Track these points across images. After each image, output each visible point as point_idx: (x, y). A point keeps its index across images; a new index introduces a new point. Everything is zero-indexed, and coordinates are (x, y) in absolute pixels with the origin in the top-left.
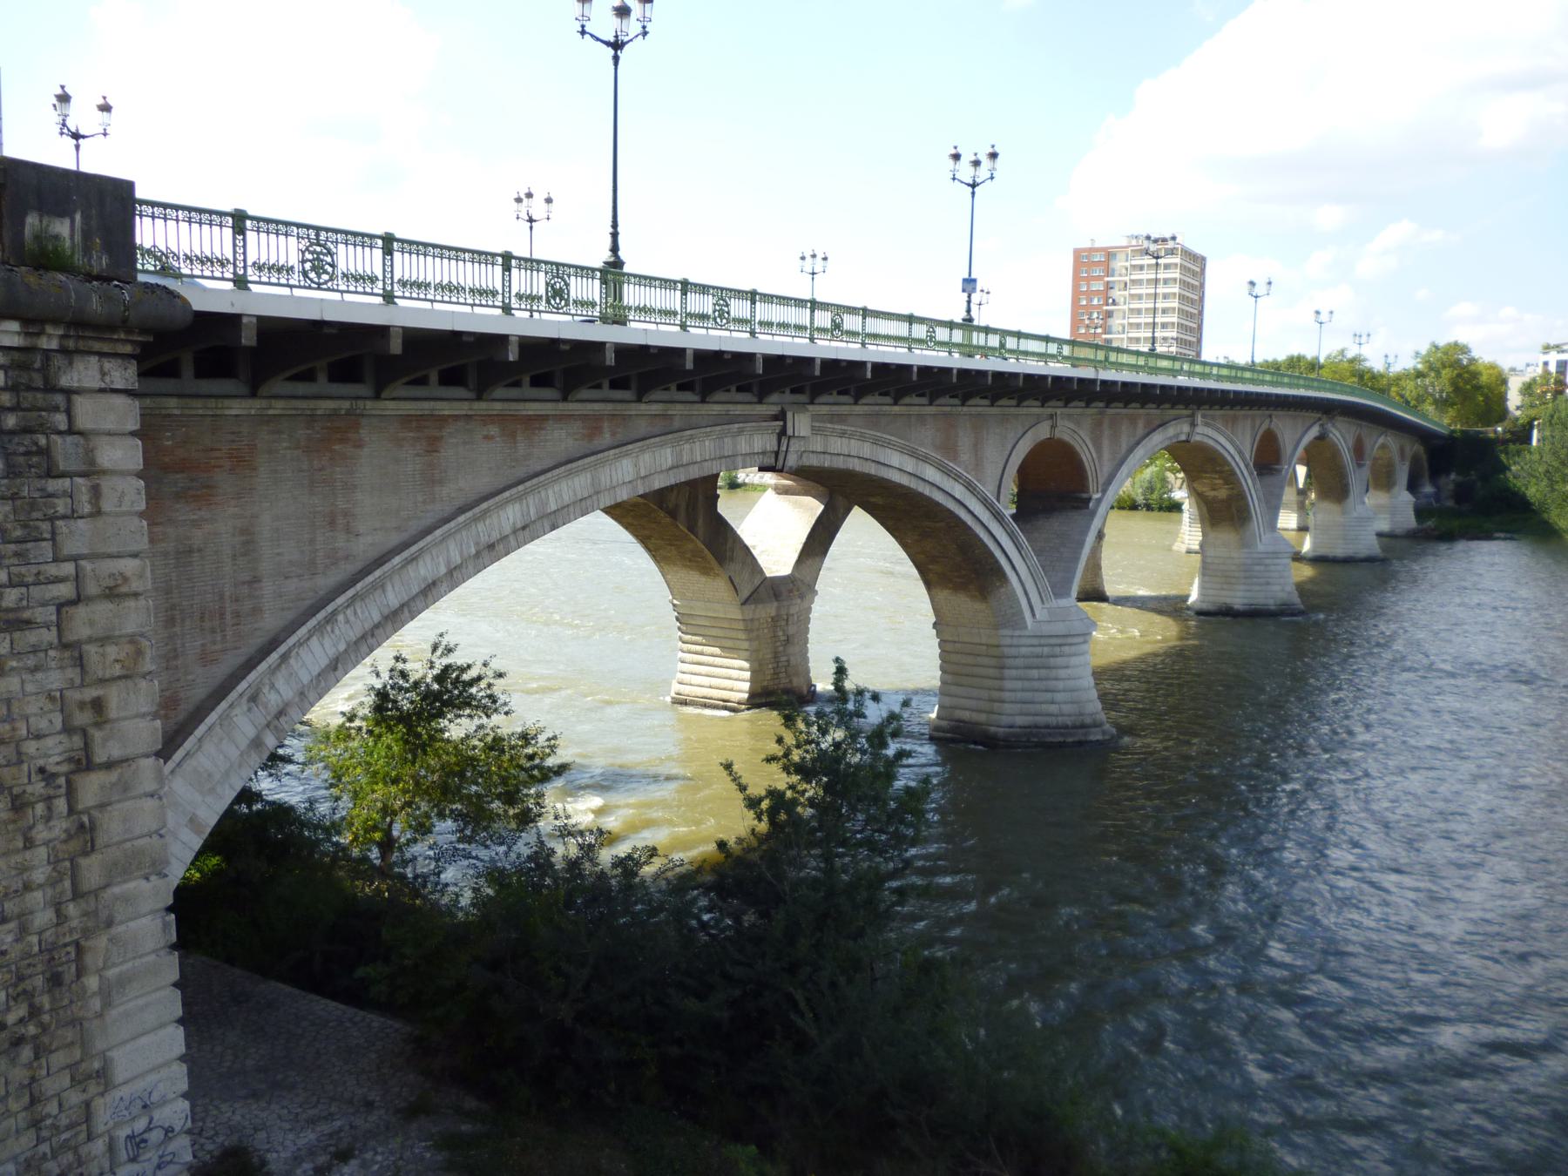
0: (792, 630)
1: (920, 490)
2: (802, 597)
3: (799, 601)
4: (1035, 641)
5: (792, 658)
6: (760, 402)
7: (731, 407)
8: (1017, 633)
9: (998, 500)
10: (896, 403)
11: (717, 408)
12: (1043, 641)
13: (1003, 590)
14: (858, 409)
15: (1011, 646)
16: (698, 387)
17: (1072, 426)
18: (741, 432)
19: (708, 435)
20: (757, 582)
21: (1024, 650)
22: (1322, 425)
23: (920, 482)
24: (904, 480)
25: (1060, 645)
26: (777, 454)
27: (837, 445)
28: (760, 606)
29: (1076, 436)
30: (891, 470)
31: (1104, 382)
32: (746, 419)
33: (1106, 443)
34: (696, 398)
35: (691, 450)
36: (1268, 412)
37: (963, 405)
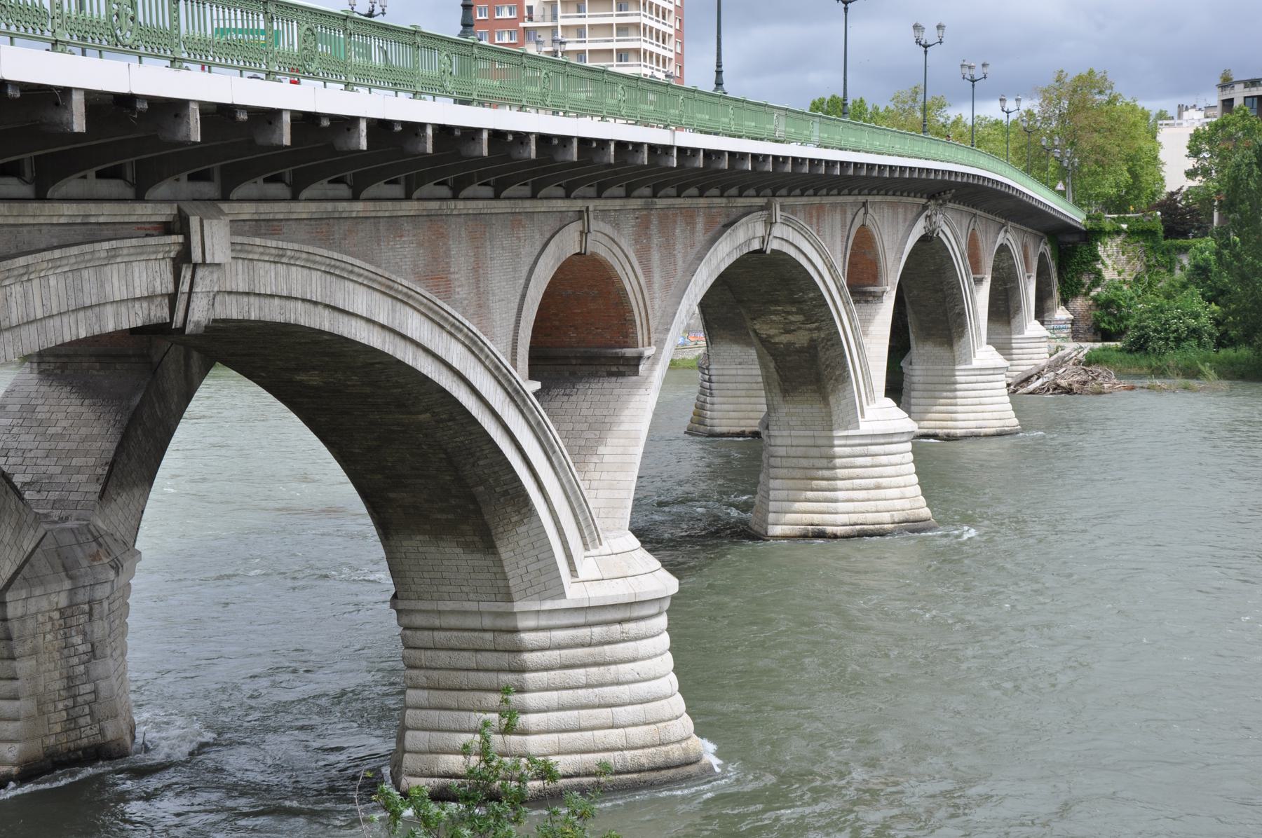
1: (399, 356)
5: (102, 685)
6: (140, 198)
7: (92, 208)
8: (548, 605)
10: (355, 197)
11: (68, 211)
12: (592, 617)
13: (522, 529)
14: (301, 209)
16: (28, 173)
17: (608, 229)
18: (112, 255)
22: (928, 217)
23: (398, 340)
26: (173, 298)
27: (270, 278)
28: (38, 591)
29: (616, 249)
30: (354, 322)
32: (116, 231)
33: (656, 256)
34: (27, 190)
35: (25, 296)
36: (861, 199)
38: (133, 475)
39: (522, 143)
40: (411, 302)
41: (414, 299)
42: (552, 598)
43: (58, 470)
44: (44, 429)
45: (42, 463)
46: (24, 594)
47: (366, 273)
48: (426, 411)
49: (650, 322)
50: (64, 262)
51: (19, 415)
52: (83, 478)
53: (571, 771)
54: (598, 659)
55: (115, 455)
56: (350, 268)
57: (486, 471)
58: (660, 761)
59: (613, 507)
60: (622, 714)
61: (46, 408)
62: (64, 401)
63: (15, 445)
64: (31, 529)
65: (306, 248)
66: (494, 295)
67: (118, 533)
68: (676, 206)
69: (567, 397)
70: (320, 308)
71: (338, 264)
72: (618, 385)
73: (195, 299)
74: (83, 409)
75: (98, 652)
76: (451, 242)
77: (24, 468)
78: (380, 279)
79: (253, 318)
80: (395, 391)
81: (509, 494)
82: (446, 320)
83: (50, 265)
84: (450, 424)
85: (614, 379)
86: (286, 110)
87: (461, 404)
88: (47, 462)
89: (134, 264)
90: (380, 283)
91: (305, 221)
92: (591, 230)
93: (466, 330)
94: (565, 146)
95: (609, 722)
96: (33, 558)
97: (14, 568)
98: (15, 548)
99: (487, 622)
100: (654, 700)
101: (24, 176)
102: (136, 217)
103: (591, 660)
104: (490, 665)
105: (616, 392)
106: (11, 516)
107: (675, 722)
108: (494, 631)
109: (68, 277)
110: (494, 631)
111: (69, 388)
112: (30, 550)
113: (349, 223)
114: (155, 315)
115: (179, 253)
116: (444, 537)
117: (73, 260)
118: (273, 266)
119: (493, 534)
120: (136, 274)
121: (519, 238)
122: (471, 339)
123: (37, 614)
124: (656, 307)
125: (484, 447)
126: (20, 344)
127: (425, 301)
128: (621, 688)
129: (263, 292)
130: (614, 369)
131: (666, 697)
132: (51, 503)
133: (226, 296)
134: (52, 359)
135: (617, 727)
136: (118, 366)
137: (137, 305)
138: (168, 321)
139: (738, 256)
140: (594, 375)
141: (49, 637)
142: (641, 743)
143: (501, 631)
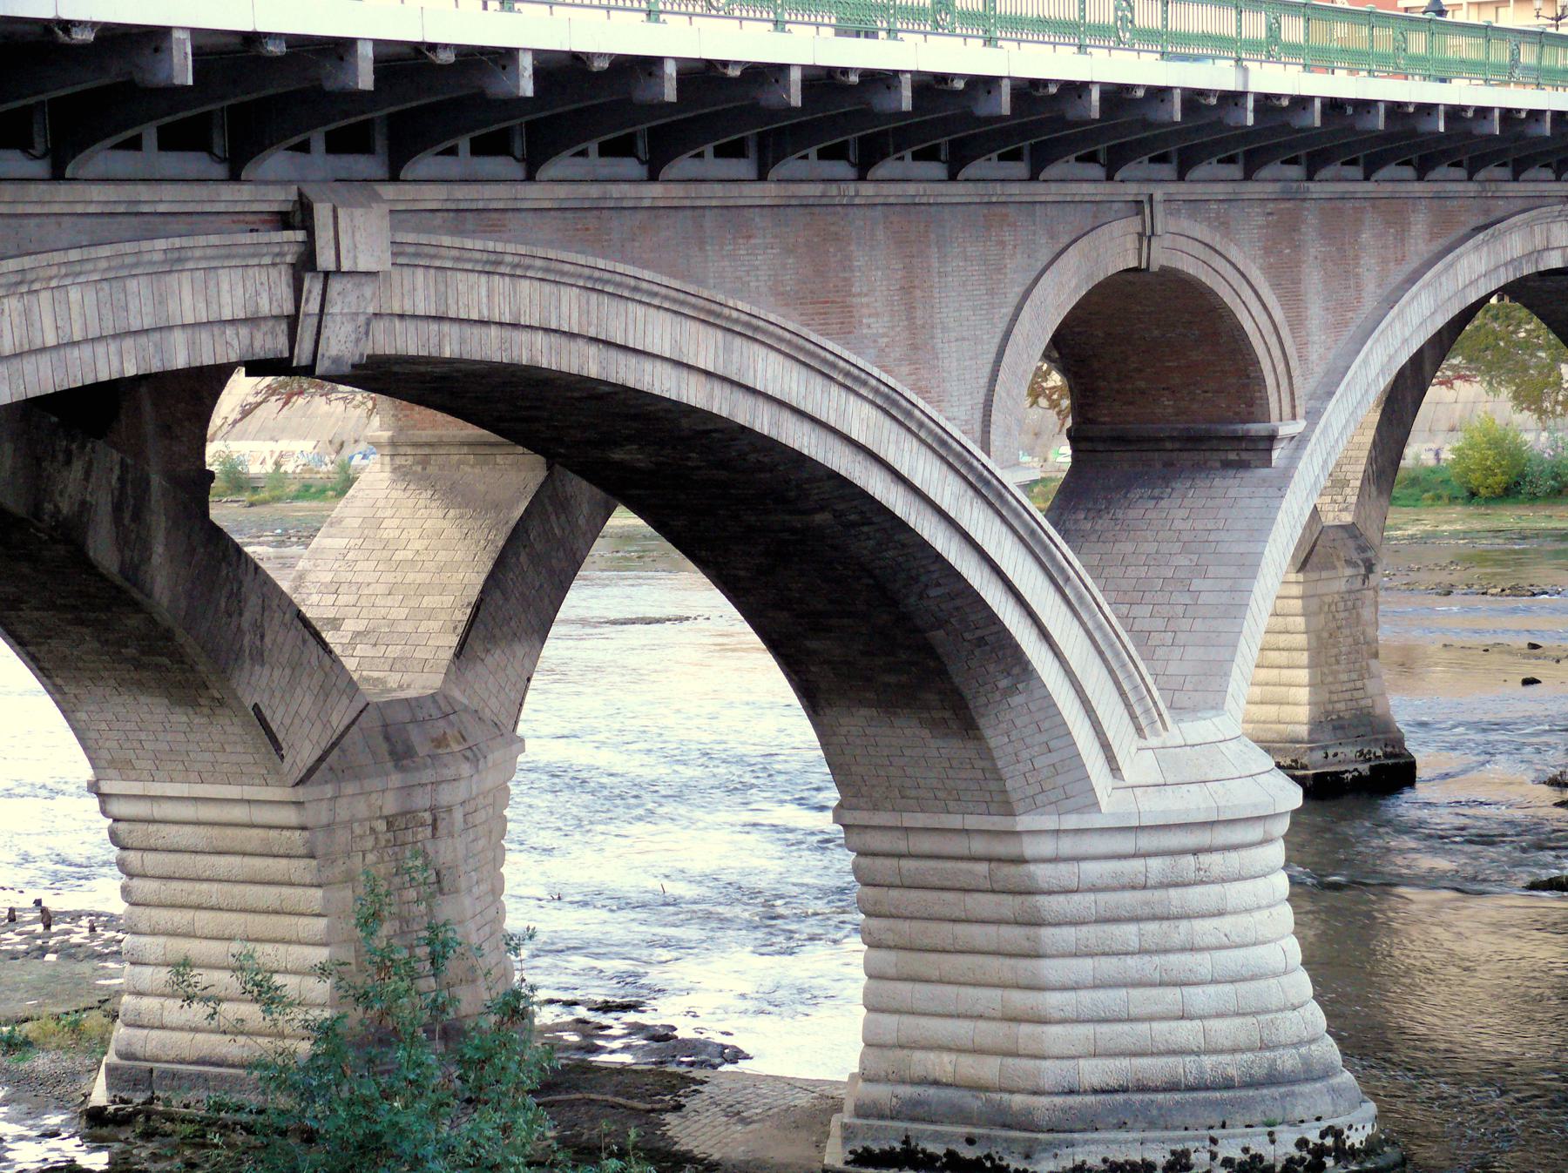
0: (447, 851)
1: (742, 418)
2: (474, 756)
3: (466, 769)
4: (1125, 844)
7: (143, 192)
8: (1071, 822)
9: (986, 449)
12: (1147, 842)
13: (1017, 700)
14: (534, 193)
15: (1056, 859)
17: (1200, 231)
18: (174, 263)
19: (73, 271)
20: (339, 719)
21: (1093, 871)
23: (739, 395)
24: (693, 393)
25: (1196, 852)
26: (293, 322)
28: (350, 788)
30: (648, 365)
31: (1266, 102)
34: (40, 168)
35: (27, 312)
37: (862, 178)
38: (513, 624)
39: (889, 88)
40: (758, 337)
41: (765, 332)
42: (1078, 810)
43: (403, 613)
44: (390, 553)
45: (382, 603)
46: (329, 790)
47: (663, 291)
48: (822, 509)
49: (1295, 381)
50: (89, 266)
51: (358, 533)
52: (434, 625)
53: (1113, 1083)
54: (1158, 910)
55: (482, 592)
56: (632, 282)
57: (943, 606)
58: (1259, 1073)
59: (1205, 674)
60: (1200, 998)
61: (396, 522)
62: (420, 513)
63: (349, 576)
64: (344, 697)
65: (540, 252)
66: (945, 329)
67: (487, 710)
68: (1359, 195)
69: (1153, 502)
70: (581, 343)
71: (607, 276)
72: (1237, 481)
73: (330, 324)
74: (445, 524)
75: (445, 884)
76: (853, 247)
77: (358, 610)
78: (693, 300)
79: (447, 355)
80: (762, 476)
81: (986, 644)
82: (833, 366)
83: (63, 271)
84: (865, 529)
85: (1231, 473)
86: (525, 49)
87: (872, 498)
88: (389, 601)
89: (220, 272)
90: (694, 307)
91: (552, 213)
92: (1159, 229)
93: (874, 382)
94: (989, 92)
95: (1176, 1009)
96: (346, 740)
97: (318, 753)
98: (318, 725)
99: (979, 846)
100: (1253, 978)
101: (33, 148)
102: (223, 205)
103: (1147, 911)
104: (985, 915)
105: (1232, 493)
106: (311, 676)
107: (1289, 1014)
108: (990, 860)
109: (102, 289)
110: (990, 860)
111: (430, 493)
112: (342, 728)
113: (640, 215)
114: (263, 347)
115: (301, 255)
116: (899, 710)
117: (103, 264)
118: (484, 278)
119: (971, 707)
120: (225, 287)
121: (1002, 244)
122: (887, 398)
123: (352, 821)
124: (1314, 357)
125: (932, 568)
126: (21, 382)
127: (788, 336)
128: (1198, 957)
129: (463, 316)
130: (1232, 456)
131: (1275, 975)
132: (390, 661)
133: (397, 322)
134: (409, 450)
135: (1191, 1018)
136: (499, 459)
137: (230, 331)
138: (286, 355)
139: (1511, 279)
140: (1200, 468)
141: (371, 858)
142: (1228, 1044)
143: (1000, 860)
